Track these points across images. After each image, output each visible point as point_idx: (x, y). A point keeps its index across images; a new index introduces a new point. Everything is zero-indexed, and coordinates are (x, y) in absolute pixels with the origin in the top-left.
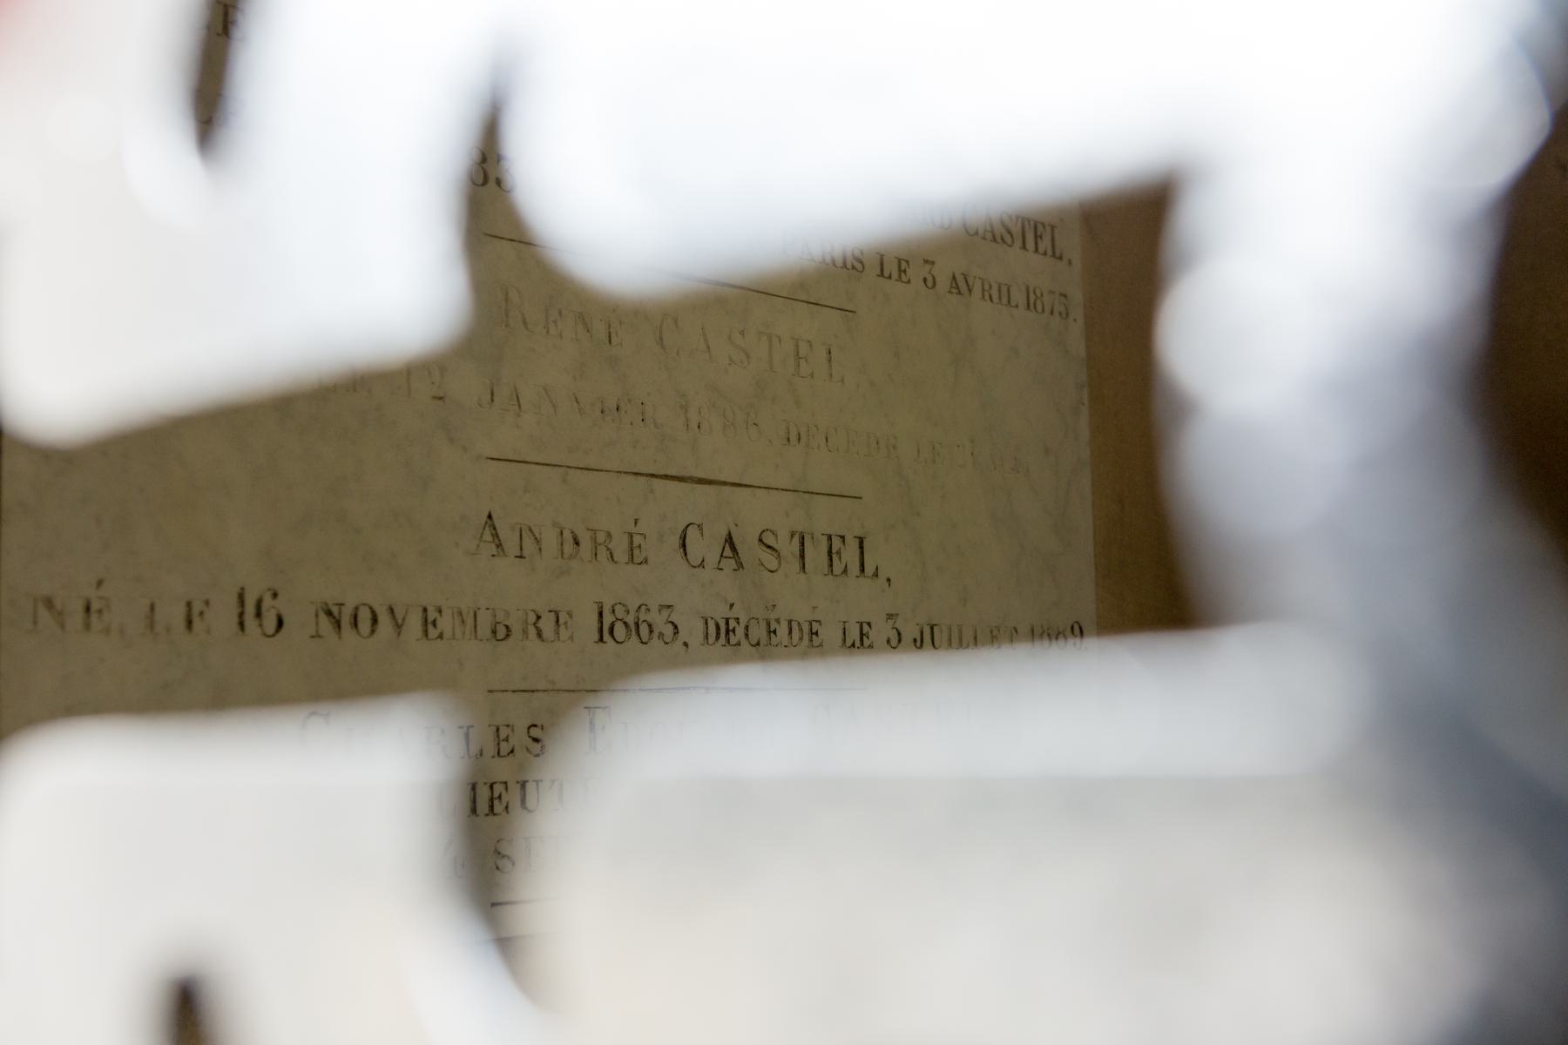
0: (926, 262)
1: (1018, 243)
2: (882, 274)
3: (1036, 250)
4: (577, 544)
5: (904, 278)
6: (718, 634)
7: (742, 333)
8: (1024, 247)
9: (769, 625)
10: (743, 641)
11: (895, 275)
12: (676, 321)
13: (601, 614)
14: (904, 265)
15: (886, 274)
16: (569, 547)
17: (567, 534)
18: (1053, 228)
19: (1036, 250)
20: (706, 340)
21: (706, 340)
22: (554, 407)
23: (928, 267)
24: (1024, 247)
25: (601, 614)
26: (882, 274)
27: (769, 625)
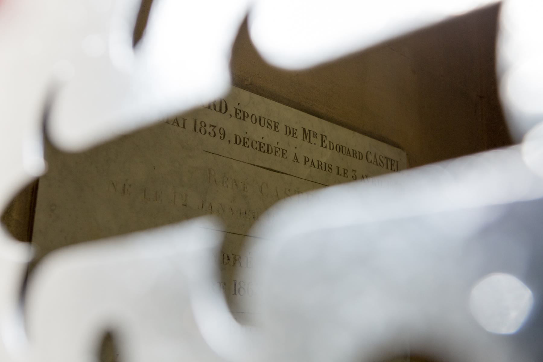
0: (353, 170)
1: (385, 166)
2: (338, 173)
3: (391, 169)
4: (229, 259)
5: (346, 175)
6: (241, 141)
7: (289, 190)
8: (387, 168)
9: (260, 144)
10: (250, 146)
11: (343, 174)
12: (267, 185)
13: (195, 124)
14: (346, 171)
15: (340, 174)
16: (226, 260)
17: (226, 256)
18: (397, 162)
19: (391, 169)
20: (277, 192)
21: (277, 192)
22: (224, 211)
23: (354, 172)
24: (387, 168)
25: (195, 124)
26: (338, 173)
27: (260, 144)
